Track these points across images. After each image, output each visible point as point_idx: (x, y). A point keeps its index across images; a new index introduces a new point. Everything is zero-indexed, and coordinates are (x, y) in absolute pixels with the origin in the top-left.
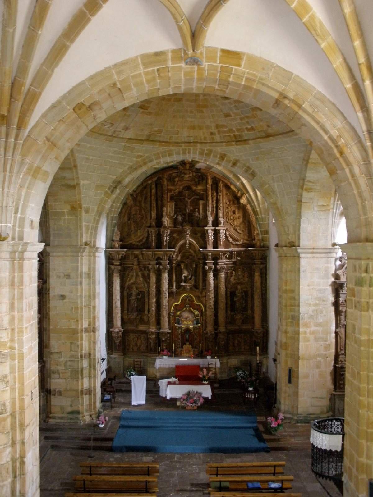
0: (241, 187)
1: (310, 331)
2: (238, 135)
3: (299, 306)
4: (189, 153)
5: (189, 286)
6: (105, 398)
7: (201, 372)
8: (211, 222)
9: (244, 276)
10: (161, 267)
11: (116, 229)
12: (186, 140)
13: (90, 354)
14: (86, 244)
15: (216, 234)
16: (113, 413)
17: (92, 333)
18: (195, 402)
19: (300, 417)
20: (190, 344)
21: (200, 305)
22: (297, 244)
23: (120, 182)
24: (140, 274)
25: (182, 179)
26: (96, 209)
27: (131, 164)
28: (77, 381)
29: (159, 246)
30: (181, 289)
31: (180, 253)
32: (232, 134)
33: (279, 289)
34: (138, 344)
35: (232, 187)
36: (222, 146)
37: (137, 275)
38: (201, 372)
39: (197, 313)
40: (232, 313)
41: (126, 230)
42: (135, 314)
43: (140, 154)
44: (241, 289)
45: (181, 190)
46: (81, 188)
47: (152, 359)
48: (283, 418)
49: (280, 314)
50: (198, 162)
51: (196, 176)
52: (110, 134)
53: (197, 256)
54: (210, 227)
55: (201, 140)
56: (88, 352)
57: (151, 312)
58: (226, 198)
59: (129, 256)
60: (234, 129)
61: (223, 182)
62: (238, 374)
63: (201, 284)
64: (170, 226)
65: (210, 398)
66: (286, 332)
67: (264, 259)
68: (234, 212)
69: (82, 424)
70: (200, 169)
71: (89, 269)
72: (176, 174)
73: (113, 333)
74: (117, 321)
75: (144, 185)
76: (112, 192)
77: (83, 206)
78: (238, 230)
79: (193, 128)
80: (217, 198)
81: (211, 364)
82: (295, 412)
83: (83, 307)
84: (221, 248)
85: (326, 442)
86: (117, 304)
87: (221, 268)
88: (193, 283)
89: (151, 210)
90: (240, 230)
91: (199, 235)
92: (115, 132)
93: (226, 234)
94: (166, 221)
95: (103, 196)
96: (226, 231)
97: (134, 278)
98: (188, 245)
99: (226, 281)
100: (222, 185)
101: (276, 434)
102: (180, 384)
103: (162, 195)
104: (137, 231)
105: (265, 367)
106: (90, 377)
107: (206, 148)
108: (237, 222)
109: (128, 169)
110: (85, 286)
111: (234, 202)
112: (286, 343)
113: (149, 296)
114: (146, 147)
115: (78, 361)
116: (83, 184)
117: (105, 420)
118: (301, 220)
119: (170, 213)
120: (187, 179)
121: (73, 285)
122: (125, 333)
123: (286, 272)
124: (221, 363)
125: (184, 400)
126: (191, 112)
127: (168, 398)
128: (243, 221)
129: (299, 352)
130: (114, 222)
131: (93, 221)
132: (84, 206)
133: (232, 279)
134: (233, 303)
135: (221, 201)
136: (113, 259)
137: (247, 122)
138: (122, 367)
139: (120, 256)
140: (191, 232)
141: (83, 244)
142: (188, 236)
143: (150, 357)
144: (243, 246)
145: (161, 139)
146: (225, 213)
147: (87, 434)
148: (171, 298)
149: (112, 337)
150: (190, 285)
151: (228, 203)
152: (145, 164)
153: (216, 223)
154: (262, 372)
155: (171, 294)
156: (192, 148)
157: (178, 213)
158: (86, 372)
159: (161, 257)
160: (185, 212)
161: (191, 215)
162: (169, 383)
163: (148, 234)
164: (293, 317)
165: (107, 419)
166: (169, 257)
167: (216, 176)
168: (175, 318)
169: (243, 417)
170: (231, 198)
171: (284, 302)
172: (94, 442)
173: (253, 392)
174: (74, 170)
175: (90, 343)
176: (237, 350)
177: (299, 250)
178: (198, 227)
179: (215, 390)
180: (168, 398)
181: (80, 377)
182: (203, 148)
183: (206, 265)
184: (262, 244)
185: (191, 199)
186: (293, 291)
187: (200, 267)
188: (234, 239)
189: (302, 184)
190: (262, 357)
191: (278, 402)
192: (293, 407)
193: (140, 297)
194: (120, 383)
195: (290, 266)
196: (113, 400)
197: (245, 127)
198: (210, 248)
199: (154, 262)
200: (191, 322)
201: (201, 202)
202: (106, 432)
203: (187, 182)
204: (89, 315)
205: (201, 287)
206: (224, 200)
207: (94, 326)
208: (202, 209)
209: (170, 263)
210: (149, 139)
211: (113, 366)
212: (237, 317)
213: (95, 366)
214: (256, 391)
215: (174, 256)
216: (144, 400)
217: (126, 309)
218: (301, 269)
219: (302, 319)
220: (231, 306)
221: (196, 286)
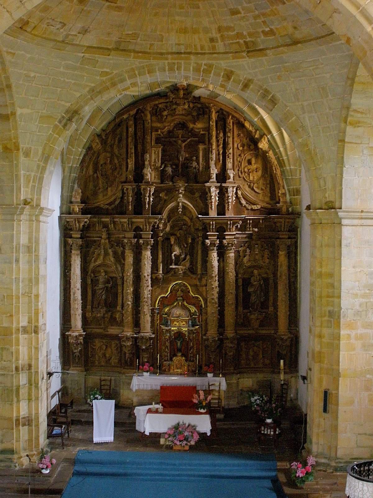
0: (260, 124)
1: (356, 334)
2: (249, 41)
3: (339, 297)
4: (179, 69)
5: (182, 270)
6: (54, 432)
7: (196, 396)
8: (214, 176)
9: (263, 256)
10: (141, 241)
11: (76, 186)
12: (174, 50)
13: (30, 366)
14: (26, 203)
15: (223, 192)
16: (64, 453)
17: (33, 334)
18: (186, 439)
19: (341, 463)
20: (183, 355)
21: (198, 297)
22: (337, 205)
23: (76, 112)
24: (110, 251)
25: (173, 113)
26: (40, 152)
27: (93, 85)
28: (11, 404)
29: (139, 209)
30: (170, 275)
31: (169, 222)
32: (241, 41)
33: (311, 273)
34: (107, 355)
35: (247, 124)
36: (228, 58)
37: (106, 254)
38: (196, 396)
39: (193, 309)
40: (245, 311)
41: (91, 186)
42: (103, 311)
43: (105, 70)
44: (259, 275)
45: (171, 129)
46: (18, 118)
47: (127, 376)
48: (315, 463)
49: (312, 310)
50: (197, 87)
51: (194, 107)
52: (61, 39)
53: (194, 225)
54: (213, 182)
55: (196, 49)
56: (27, 363)
57: (125, 308)
58: (239, 141)
59: (94, 225)
60: (245, 33)
61: (233, 117)
62: (253, 400)
63: (199, 266)
64: (155, 181)
65: (209, 434)
66: (320, 336)
67: (294, 231)
68: (249, 162)
69: (17, 468)
70: (200, 97)
71: (30, 239)
72: (165, 104)
73: (69, 338)
74: (75, 319)
75: (117, 120)
76: (65, 126)
77: (21, 146)
78: (255, 188)
79: (184, 31)
80: (224, 140)
81: (212, 385)
82: (333, 454)
83: (21, 296)
84: (230, 214)
85: (368, 494)
86: (76, 295)
87: (228, 244)
88: (188, 264)
89: (127, 158)
90: (258, 188)
91: (197, 195)
92: (67, 36)
93: (236, 193)
94: (149, 175)
95: (51, 132)
96: (237, 190)
97: (102, 257)
98: (180, 210)
99: (236, 263)
100: (231, 121)
101: (304, 487)
102: (164, 412)
103: (144, 136)
104: (107, 188)
105: (293, 391)
106: (30, 400)
107: (204, 61)
108: (255, 176)
109: (89, 92)
110: (23, 265)
111: (249, 146)
112: (320, 353)
113: (123, 284)
114: (114, 59)
115: (12, 375)
116: (21, 114)
117: (52, 464)
118: (344, 169)
119: (155, 162)
120: (181, 113)
121: (6, 262)
122: (88, 338)
123: (322, 246)
124: (228, 384)
125: (170, 436)
126: (181, 7)
127: (147, 433)
128: (263, 176)
129: (339, 365)
130: (73, 175)
131: (35, 168)
132: (23, 146)
133: (245, 260)
134: (247, 296)
135: (231, 145)
136: (71, 230)
137: (264, 22)
138: (83, 390)
139: (82, 224)
140: (185, 190)
141: (22, 202)
142: (181, 195)
143: (124, 373)
144: (262, 211)
145: (138, 48)
146: (236, 163)
147: (23, 484)
148: (155, 287)
149: (68, 343)
150: (184, 268)
151: (241, 148)
152: (114, 85)
153: (222, 177)
154: (289, 399)
155: (155, 281)
156: (183, 62)
157: (166, 162)
158: (23, 392)
159: (141, 227)
160: (177, 162)
161: (186, 166)
162: (149, 411)
163: (123, 193)
164: (331, 314)
165: (54, 461)
166: (154, 226)
167: (223, 107)
168: (161, 317)
169: (259, 462)
170: (245, 141)
171: (318, 290)
172: (33, 495)
173: (272, 425)
174: (7, 93)
175: (30, 348)
176: (252, 365)
177: (341, 214)
178: (196, 181)
179: (218, 423)
180: (147, 433)
181: (15, 399)
182: (200, 62)
183: (208, 239)
184: (290, 209)
185: (187, 142)
186: (331, 275)
187: (198, 242)
188: (249, 202)
189: (345, 114)
190: (288, 376)
191: (308, 440)
192: (330, 448)
193: (109, 285)
194: (79, 411)
195: (326, 238)
196: (67, 435)
197: (260, 30)
198: (213, 213)
199: (131, 234)
200: (184, 323)
201: (201, 147)
202: (52, 480)
203: (181, 117)
204: (30, 308)
205: (199, 272)
206: (235, 143)
207: (37, 324)
208: (203, 157)
209: (155, 236)
210: (120, 48)
211: (70, 386)
212: (252, 316)
213: (38, 384)
214: (277, 423)
215: (161, 226)
216: (111, 436)
217: (89, 302)
218: (344, 242)
219: (344, 317)
220: (244, 300)
221: (192, 270)
